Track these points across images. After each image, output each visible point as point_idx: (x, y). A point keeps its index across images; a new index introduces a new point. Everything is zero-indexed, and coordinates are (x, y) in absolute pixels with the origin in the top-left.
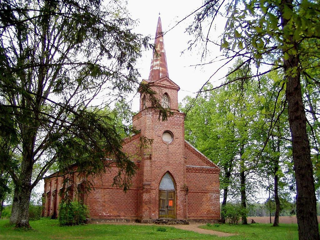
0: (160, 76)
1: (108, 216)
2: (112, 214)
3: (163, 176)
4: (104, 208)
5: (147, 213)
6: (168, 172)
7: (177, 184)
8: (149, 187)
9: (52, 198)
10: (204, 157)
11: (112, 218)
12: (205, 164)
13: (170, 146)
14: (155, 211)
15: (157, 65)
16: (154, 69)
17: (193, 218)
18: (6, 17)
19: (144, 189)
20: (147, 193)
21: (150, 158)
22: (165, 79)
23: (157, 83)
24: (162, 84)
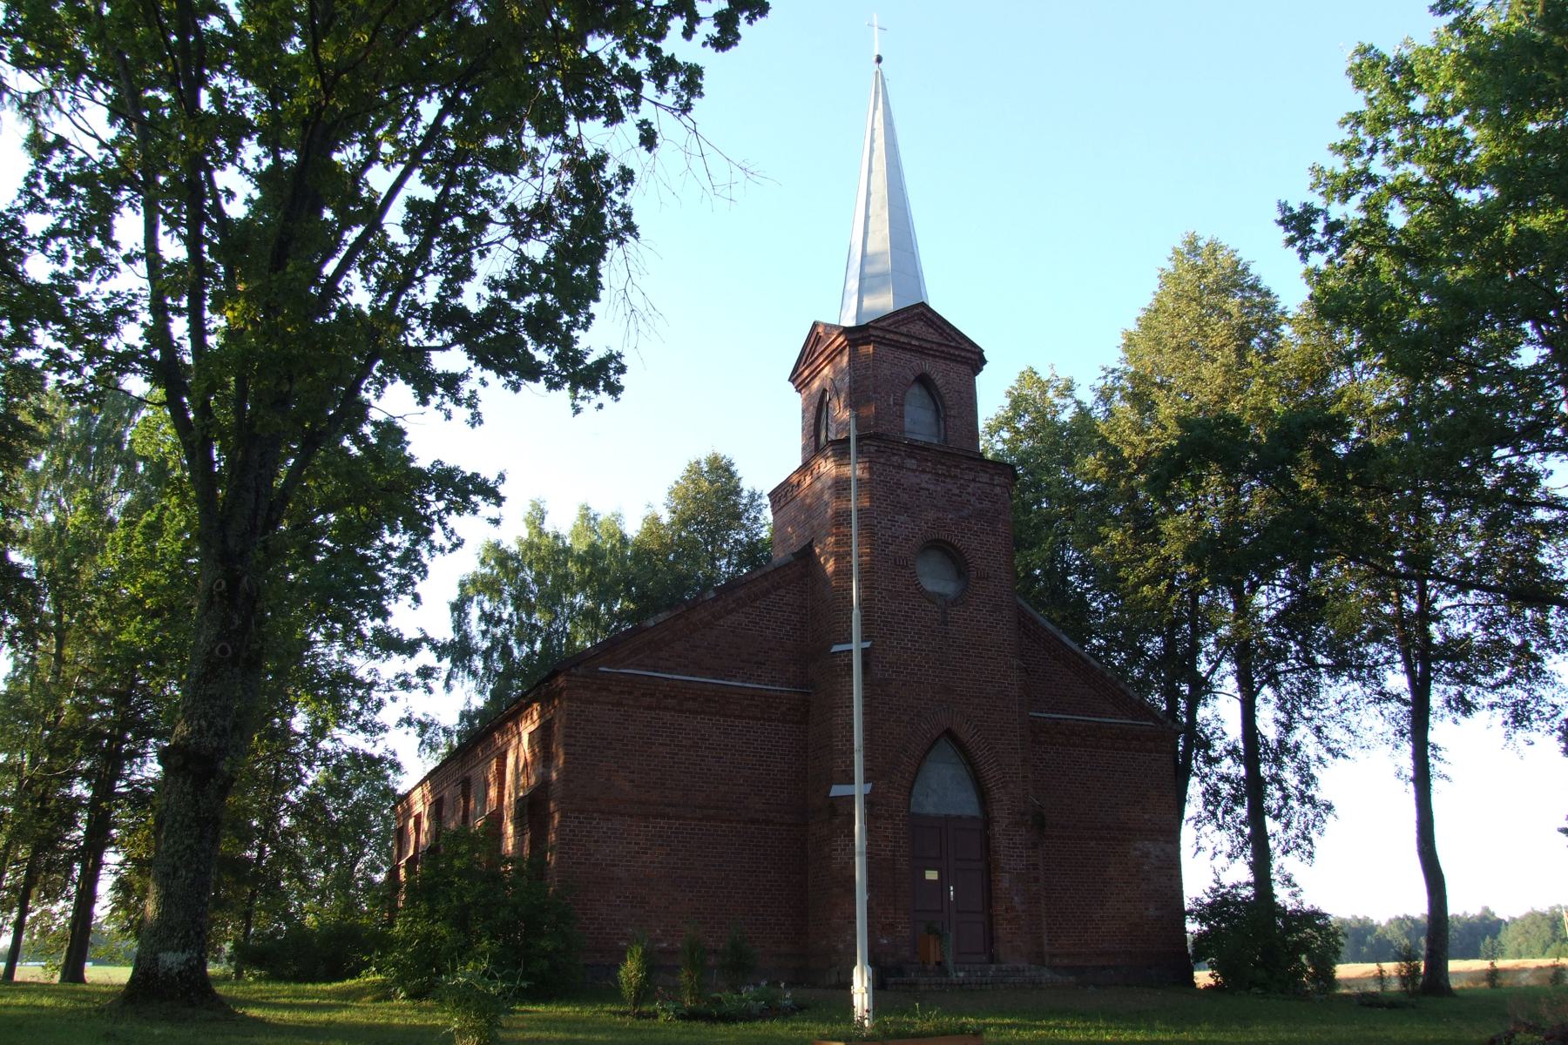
3: (927, 752)
6: (949, 734)
17: (1066, 961)
18: (932, 875)
24: (907, 336)
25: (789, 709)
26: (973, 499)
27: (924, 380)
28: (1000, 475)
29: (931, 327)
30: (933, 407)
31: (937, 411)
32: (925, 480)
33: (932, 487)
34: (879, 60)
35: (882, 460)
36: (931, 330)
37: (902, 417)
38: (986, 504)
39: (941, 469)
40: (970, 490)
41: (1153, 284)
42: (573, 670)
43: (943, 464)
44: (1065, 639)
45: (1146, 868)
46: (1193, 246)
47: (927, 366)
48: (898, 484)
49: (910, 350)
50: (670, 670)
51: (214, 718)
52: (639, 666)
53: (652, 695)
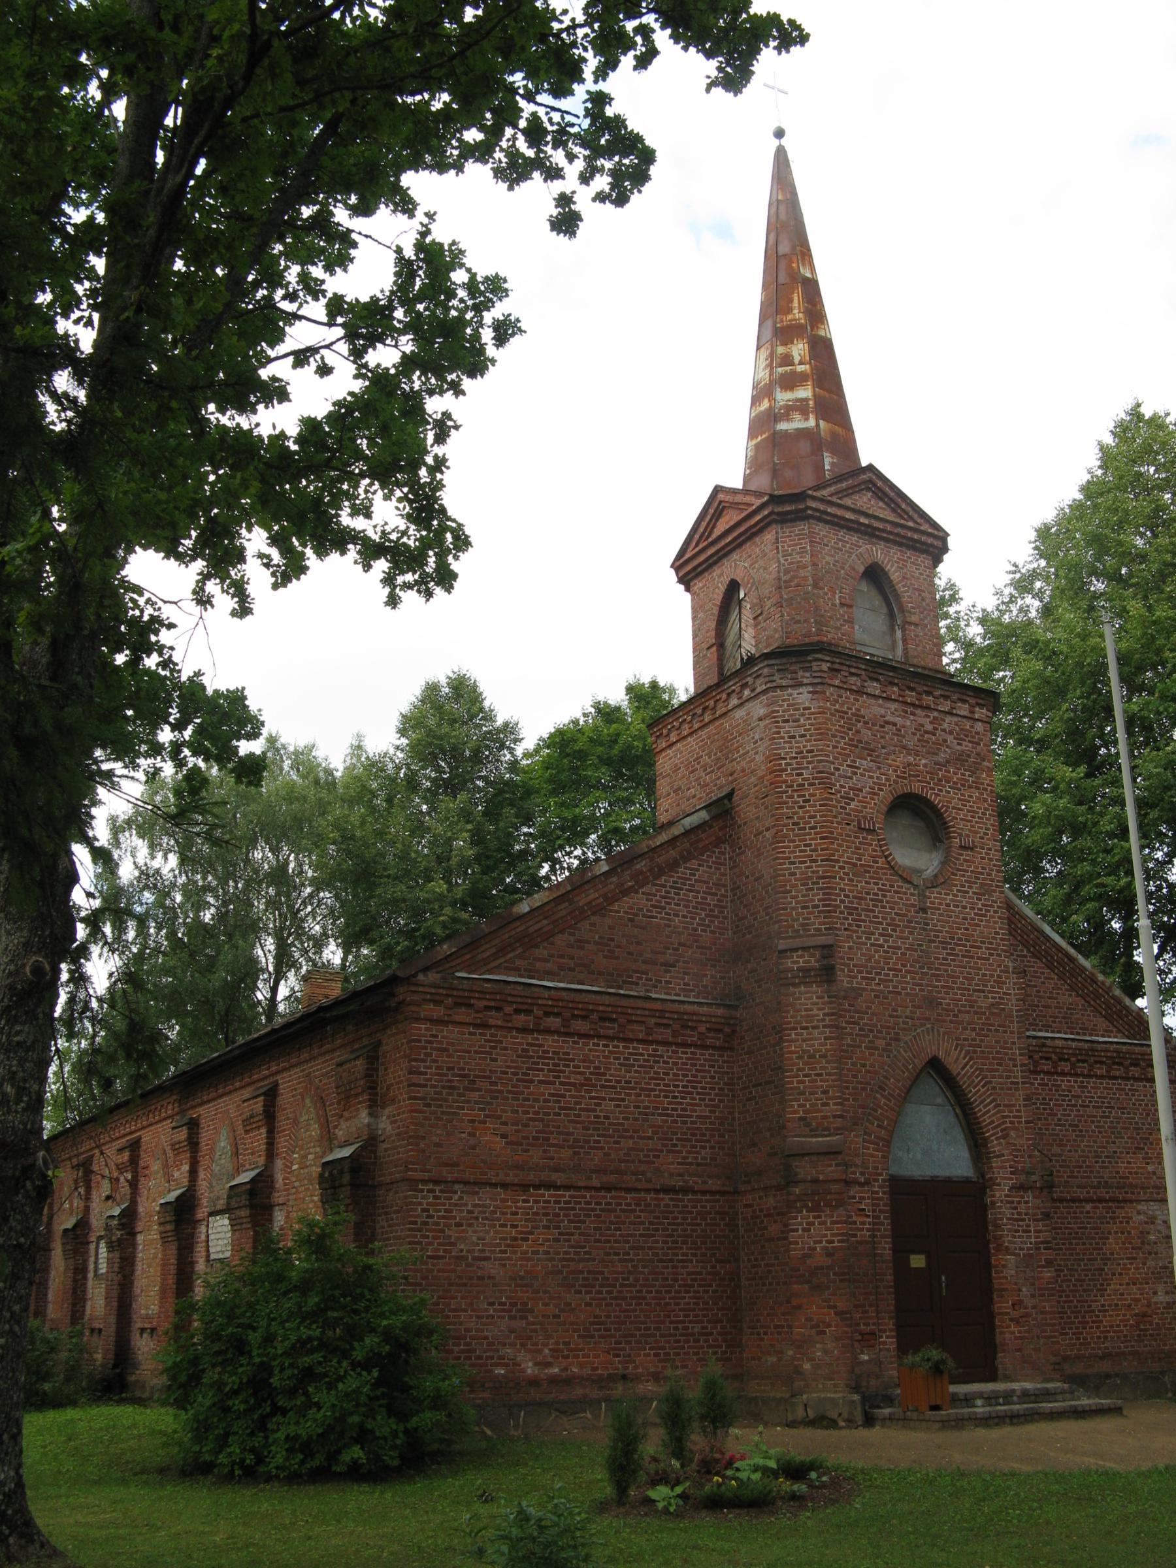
0: (827, 467)
1: (553, 1380)
2: (582, 1366)
3: (909, 1090)
4: (523, 1323)
5: (825, 1352)
6: (935, 1065)
7: (995, 1146)
8: (830, 1170)
9: (102, 1257)
10: (1094, 980)
11: (579, 1391)
12: (1102, 1023)
13: (933, 895)
14: (872, 1333)
15: (800, 407)
16: (783, 426)
19: (796, 1183)
20: (816, 1208)
21: (827, 973)
22: (865, 482)
23: (822, 500)
25: (708, 1030)
26: (950, 738)
27: (874, 575)
28: (981, 706)
29: (881, 499)
30: (885, 610)
31: (891, 615)
32: (890, 711)
33: (898, 720)
34: (779, 134)
35: (837, 682)
36: (881, 504)
37: (851, 621)
38: (966, 746)
39: (911, 697)
40: (946, 726)
41: (1092, 460)
42: (421, 977)
43: (912, 689)
44: (1047, 929)
45: (1152, 1237)
46: (1135, 413)
47: (879, 553)
48: (859, 716)
49: (857, 531)
50: (551, 975)
51: (25, 1080)
52: (509, 970)
53: (528, 1012)
